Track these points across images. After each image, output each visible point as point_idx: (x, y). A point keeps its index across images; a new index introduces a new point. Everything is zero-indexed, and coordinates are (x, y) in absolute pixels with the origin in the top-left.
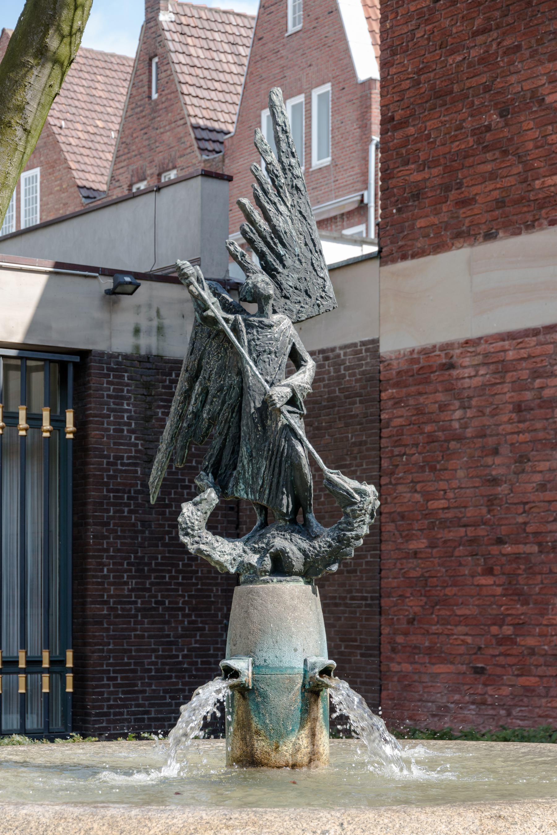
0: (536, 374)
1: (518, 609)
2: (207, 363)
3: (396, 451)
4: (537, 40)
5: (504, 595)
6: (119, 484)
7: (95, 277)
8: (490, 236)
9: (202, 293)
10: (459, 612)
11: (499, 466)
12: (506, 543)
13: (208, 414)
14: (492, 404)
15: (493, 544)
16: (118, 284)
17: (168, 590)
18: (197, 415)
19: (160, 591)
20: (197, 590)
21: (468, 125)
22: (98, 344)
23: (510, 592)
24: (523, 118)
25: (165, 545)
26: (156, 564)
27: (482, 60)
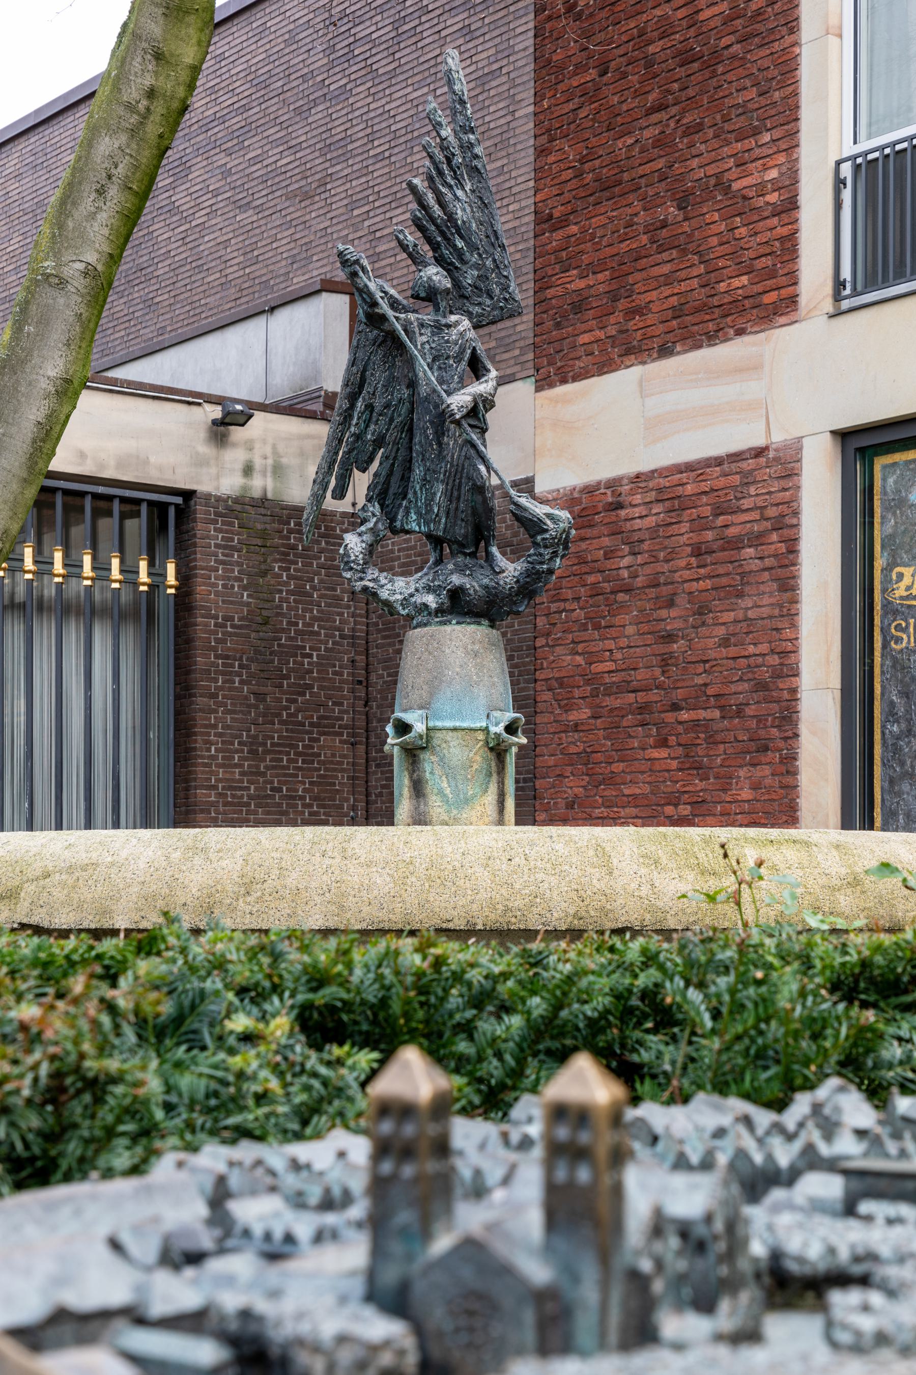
0: (719, 511)
1: (696, 785)
2: (372, 375)
3: (554, 607)
4: (723, 116)
5: (680, 770)
6: (229, 649)
7: (199, 404)
8: (665, 352)
9: (368, 283)
10: (626, 792)
11: (674, 619)
12: (682, 709)
13: (373, 434)
14: (666, 548)
15: (668, 711)
16: (227, 414)
17: (285, 775)
18: (358, 437)
19: (277, 776)
20: (319, 776)
21: (642, 218)
22: (204, 485)
23: (687, 765)
24: (705, 210)
25: (282, 722)
26: (273, 745)
27: (658, 143)
